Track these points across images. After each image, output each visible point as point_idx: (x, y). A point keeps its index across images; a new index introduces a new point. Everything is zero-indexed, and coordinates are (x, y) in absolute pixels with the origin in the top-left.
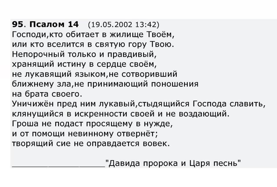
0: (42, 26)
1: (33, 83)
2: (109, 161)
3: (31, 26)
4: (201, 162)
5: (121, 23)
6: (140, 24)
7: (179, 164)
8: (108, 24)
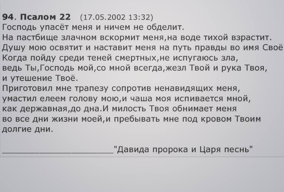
0: (33, 19)
1: (171, 66)
2: (118, 148)
3: (21, 19)
4: (212, 148)
5: (114, 16)
6: (133, 17)
7: (190, 150)
8: (101, 17)
